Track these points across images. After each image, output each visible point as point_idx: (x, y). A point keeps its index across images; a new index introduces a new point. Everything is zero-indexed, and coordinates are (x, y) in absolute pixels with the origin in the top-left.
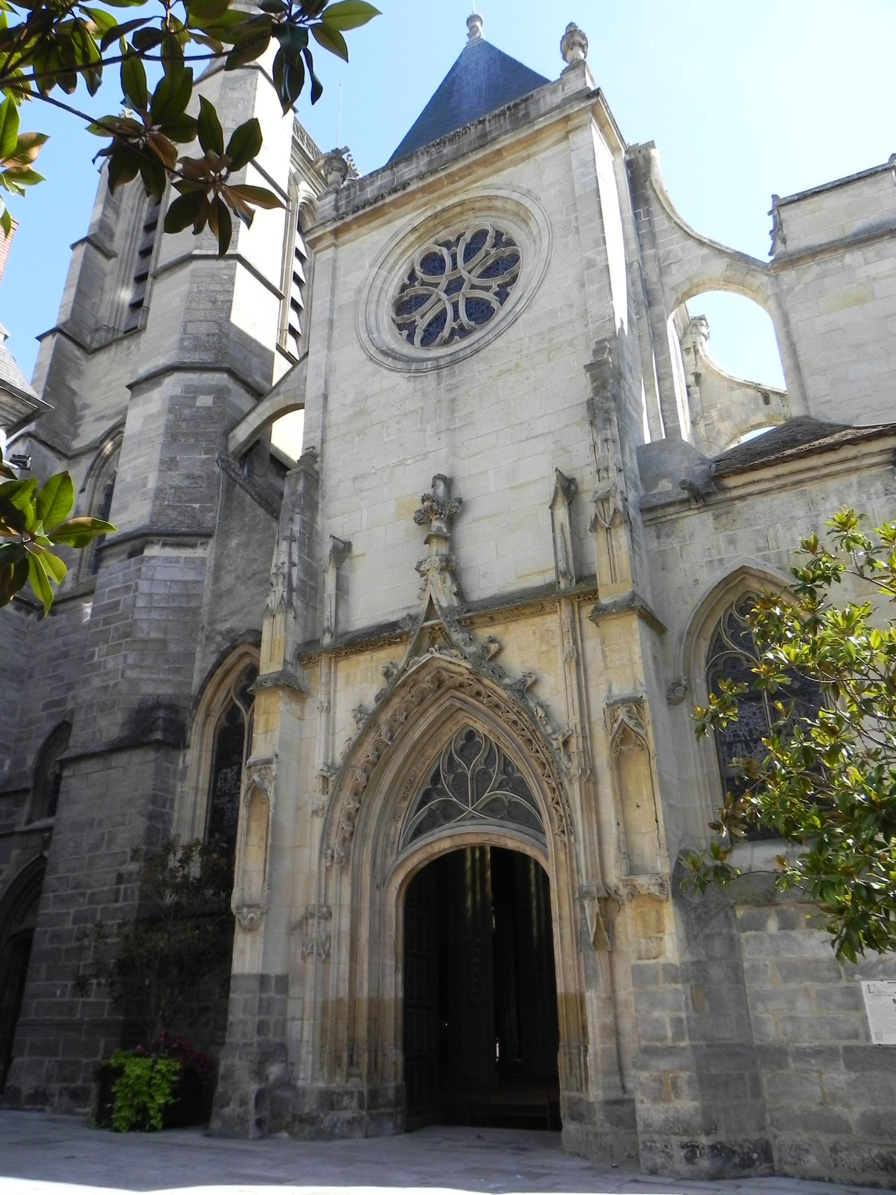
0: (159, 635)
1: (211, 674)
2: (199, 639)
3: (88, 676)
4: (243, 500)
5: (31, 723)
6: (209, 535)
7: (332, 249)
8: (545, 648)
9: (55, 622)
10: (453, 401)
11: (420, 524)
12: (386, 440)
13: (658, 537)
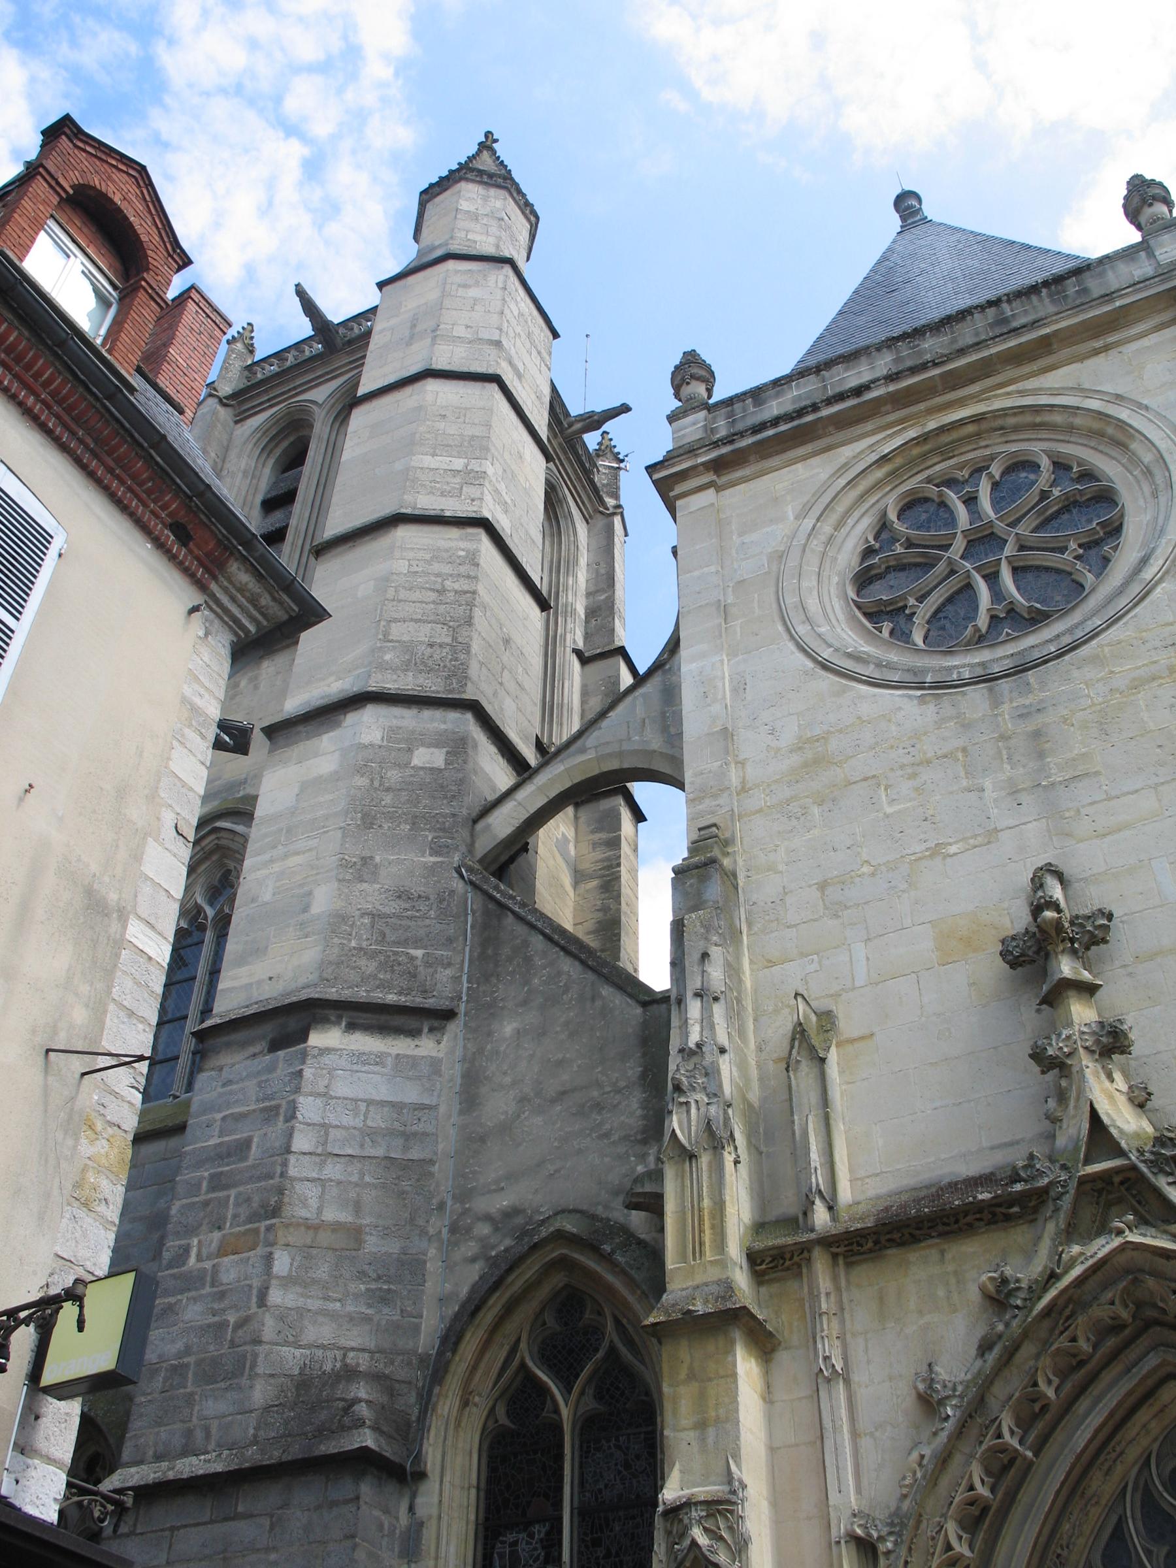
0: (345, 1217)
1: (472, 1308)
2: (431, 1231)
3: (172, 1300)
6: (449, 1015)
7: (711, 491)
11: (1014, 964)
12: (889, 810)
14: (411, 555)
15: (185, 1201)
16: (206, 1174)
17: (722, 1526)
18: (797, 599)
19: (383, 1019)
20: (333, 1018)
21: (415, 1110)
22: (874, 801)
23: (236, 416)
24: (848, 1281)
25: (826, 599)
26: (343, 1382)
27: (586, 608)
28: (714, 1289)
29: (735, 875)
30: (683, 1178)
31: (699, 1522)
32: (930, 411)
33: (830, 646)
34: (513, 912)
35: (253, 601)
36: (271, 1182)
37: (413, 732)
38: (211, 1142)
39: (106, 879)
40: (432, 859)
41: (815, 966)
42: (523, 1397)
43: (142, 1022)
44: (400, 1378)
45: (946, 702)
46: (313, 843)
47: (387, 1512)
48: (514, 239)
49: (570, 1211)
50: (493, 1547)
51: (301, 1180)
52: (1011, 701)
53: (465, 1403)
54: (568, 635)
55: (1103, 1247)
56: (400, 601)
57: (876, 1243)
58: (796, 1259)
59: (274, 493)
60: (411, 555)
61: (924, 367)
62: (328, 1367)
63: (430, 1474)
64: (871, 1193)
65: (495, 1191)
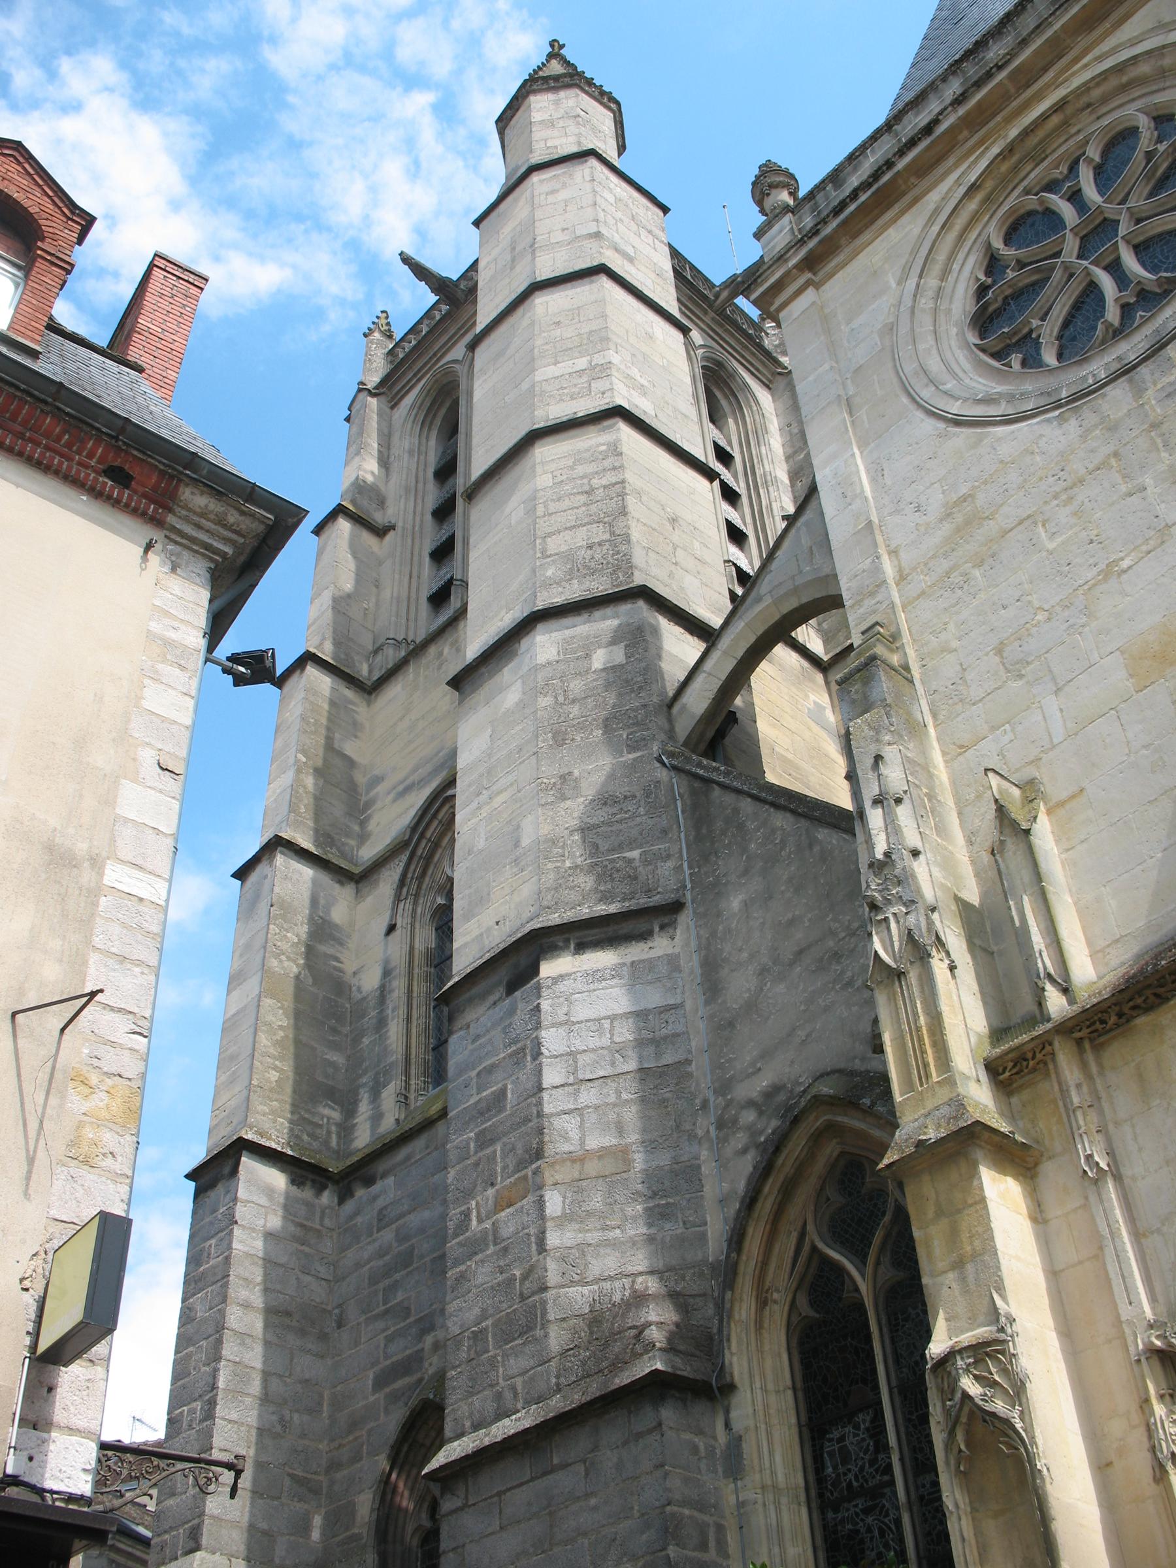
0: (610, 1140)
1: (751, 1201)
2: (700, 1133)
5: (354, 1425)
6: (676, 907)
7: (810, 291)
9: (375, 1198)
12: (1051, 546)
14: (553, 467)
15: (457, 1168)
16: (472, 1134)
17: (993, 1370)
18: (916, 364)
19: (610, 930)
20: (561, 944)
21: (661, 1013)
22: (1034, 541)
23: (389, 402)
24: (1101, 1066)
25: (948, 355)
26: (633, 1309)
27: (789, 473)
28: (945, 1110)
29: (907, 668)
30: (895, 999)
31: (967, 1371)
32: (1009, 120)
33: (957, 399)
34: (719, 784)
35: (221, 522)
36: (530, 1124)
37: (588, 637)
38: (472, 1101)
39: (71, 830)
40: (631, 756)
41: (1010, 736)
43: (138, 965)
44: (694, 1293)
45: (1086, 413)
46: (511, 778)
47: (700, 1432)
48: (595, 131)
49: (828, 1074)
50: (822, 1447)
51: (558, 1114)
52: (1155, 383)
54: (774, 504)
56: (551, 514)
57: (1120, 1015)
58: (1039, 1056)
59: (442, 463)
60: (553, 467)
61: (989, 75)
62: (617, 1298)
63: (739, 1385)
64: (1114, 963)
65: (753, 1074)
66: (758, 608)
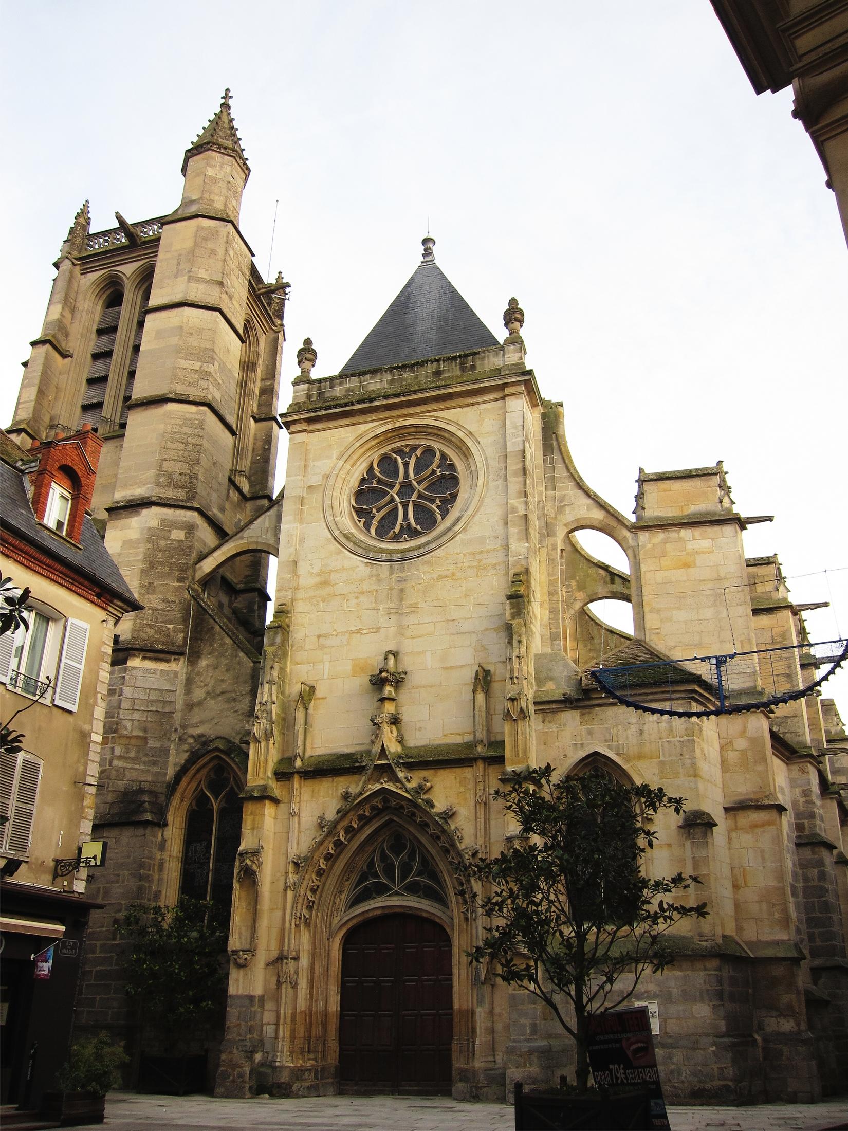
4: (213, 628)
8: (462, 789)
10: (402, 590)
11: (373, 684)
13: (543, 722)
14: (173, 421)
19: (156, 655)
42: (201, 800)
53: (182, 801)
55: (377, 787)
60: (173, 421)
66: (241, 542)
